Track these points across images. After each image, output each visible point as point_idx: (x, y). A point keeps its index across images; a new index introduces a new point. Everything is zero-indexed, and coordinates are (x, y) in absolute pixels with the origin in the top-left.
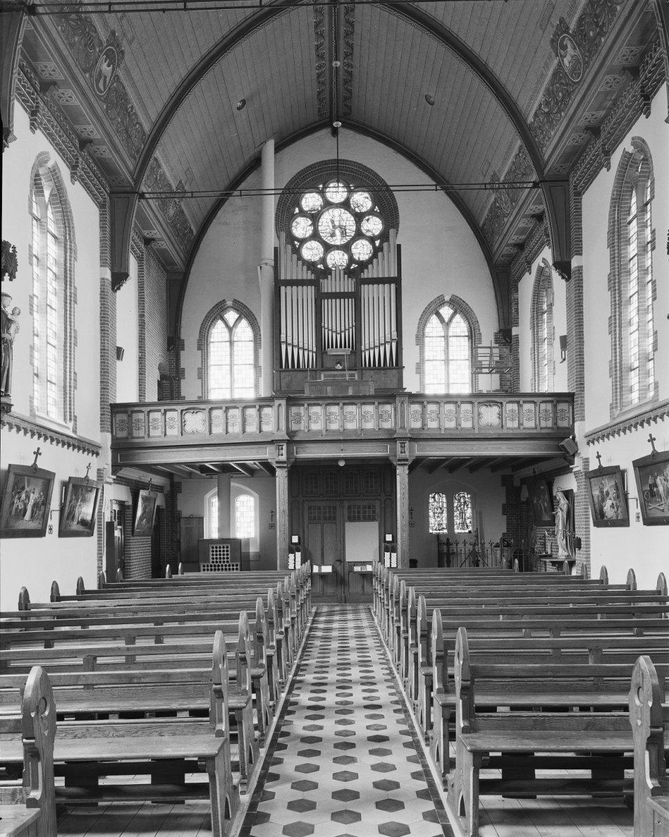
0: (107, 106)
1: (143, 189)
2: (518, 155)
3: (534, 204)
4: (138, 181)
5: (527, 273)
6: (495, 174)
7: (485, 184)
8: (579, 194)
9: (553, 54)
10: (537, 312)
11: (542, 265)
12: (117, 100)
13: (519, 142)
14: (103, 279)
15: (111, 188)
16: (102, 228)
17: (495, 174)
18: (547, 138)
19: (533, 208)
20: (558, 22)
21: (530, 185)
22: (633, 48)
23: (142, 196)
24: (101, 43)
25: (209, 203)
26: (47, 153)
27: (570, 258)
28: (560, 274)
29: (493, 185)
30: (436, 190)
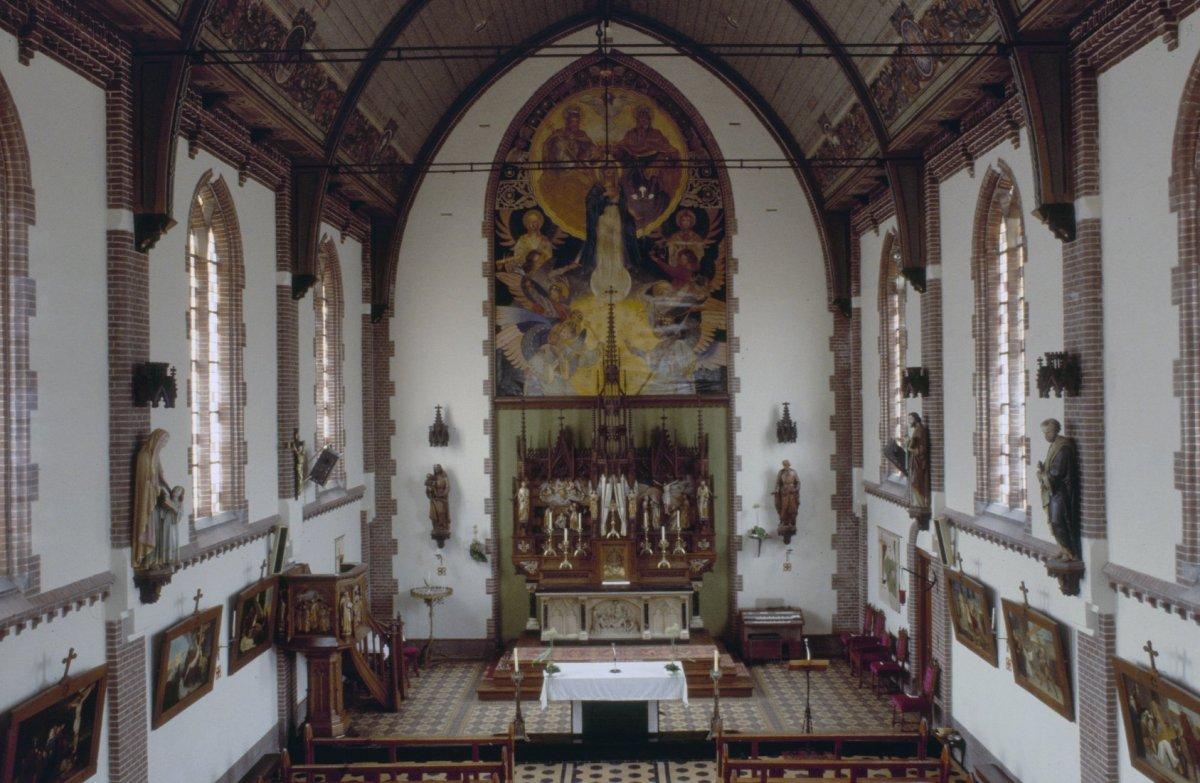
6: (824, 115)
9: (895, 32)
13: (854, 99)
14: (280, 288)
16: (364, 258)
17: (824, 115)
27: (1073, 197)
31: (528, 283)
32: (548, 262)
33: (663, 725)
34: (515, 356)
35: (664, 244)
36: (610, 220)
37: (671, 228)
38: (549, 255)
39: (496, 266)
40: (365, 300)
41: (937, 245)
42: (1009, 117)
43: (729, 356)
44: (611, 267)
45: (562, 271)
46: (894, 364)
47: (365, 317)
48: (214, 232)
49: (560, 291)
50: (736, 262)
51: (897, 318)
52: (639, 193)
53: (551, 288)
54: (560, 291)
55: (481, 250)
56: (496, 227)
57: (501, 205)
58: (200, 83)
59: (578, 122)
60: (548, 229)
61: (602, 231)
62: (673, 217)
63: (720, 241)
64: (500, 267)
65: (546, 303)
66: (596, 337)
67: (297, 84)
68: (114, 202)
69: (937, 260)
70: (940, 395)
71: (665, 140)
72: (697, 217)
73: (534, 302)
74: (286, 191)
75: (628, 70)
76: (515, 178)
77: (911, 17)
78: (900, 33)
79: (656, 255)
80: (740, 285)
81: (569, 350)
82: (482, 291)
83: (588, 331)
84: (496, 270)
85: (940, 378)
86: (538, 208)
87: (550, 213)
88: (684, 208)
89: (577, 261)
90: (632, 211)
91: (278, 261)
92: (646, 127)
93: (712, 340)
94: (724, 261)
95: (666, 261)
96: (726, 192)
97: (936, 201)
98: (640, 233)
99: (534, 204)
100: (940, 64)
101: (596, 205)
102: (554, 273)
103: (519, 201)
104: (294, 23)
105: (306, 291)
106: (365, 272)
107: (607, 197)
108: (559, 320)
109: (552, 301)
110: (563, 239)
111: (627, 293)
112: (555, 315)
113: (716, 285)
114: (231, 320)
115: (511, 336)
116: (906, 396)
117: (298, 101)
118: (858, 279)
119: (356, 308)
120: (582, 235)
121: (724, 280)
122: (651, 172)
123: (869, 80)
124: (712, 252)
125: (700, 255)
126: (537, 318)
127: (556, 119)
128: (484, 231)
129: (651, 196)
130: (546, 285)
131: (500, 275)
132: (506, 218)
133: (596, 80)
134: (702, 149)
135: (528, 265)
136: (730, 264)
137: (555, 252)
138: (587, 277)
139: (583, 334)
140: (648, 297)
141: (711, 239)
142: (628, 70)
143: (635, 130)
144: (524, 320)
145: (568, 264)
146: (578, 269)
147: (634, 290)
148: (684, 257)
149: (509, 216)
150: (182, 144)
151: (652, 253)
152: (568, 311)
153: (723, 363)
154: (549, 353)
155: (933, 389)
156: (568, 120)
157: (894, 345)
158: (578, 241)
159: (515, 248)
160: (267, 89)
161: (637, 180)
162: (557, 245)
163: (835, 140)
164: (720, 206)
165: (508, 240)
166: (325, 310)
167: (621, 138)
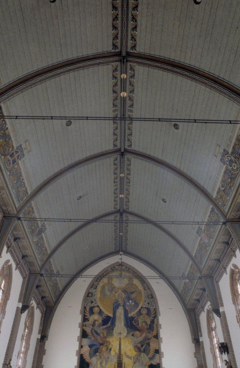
0: (10, 174)
1: (21, 216)
2: (210, 216)
3: (215, 254)
4: (18, 212)
5: (234, 258)
7: (180, 277)
8: (217, 282)
9: (198, 236)
10: (210, 330)
11: (233, 268)
12: (40, 245)
13: (191, 262)
14: (18, 308)
15: (30, 271)
16: (41, 319)
17: (183, 273)
18: (225, 202)
19: (200, 287)
20: (223, 151)
21: (198, 278)
22: (236, 213)
23: (19, 219)
24: (13, 148)
25: (68, 279)
26: (10, 260)
28: (216, 314)
29: (183, 277)
30: (160, 279)
31: (93, 331)
32: (100, 324)
33: (150, 52)
34: (87, 357)
35: (137, 319)
36: (120, 311)
37: (139, 313)
38: (101, 321)
39: (83, 324)
40: (39, 333)
41: (221, 300)
42: (232, 250)
43: (160, 359)
44: (120, 326)
45: (105, 327)
46: (217, 357)
47: (38, 339)
48: (5, 281)
49: (103, 334)
50: (160, 325)
51: (214, 332)
52: (129, 303)
53: (100, 333)
54: (103, 334)
55: (79, 319)
56: (85, 312)
57: (87, 305)
58: (15, 233)
59: (112, 281)
60: (100, 313)
61: (118, 314)
62: (140, 310)
63: (155, 318)
64: (84, 325)
65: (98, 338)
66: (115, 351)
67: (38, 244)
68: (19, 301)
69: (222, 305)
70: (233, 351)
71: (137, 287)
72: (148, 310)
73: (95, 337)
74: (26, 279)
75: (126, 267)
76: (92, 297)
77: (202, 230)
78: (200, 236)
79: (135, 323)
80: (163, 334)
81: (105, 355)
82: (77, 332)
83: (112, 348)
84: (83, 326)
85: (231, 345)
86: (98, 306)
87: (101, 308)
88: (143, 308)
89: (109, 323)
90: (127, 308)
91: (19, 299)
92: (132, 283)
93: (154, 353)
94: (157, 325)
95: (138, 325)
96: (156, 303)
97: (219, 288)
98: (129, 315)
99: (97, 305)
100: (211, 239)
101: (116, 306)
102: (102, 327)
103: (92, 304)
104: (42, 226)
105: (25, 311)
106: (41, 324)
107: (119, 304)
108: (102, 344)
109: (101, 337)
110: (105, 316)
111: (125, 334)
112: (101, 342)
113: (154, 333)
114: (2, 309)
115: (86, 350)
116: (221, 353)
117: (37, 250)
118: (201, 331)
119: (36, 335)
120: (111, 315)
121: (157, 332)
122: (133, 296)
123: (194, 255)
124: (153, 322)
125: (149, 323)
126: (95, 343)
127: (105, 280)
128: (81, 313)
129: (133, 304)
130: (99, 332)
131: (84, 328)
132: (88, 309)
133: (117, 270)
134: (148, 290)
135: (93, 325)
136: (158, 326)
137: (103, 321)
138: (113, 330)
139: (110, 349)
140: (132, 337)
141: (153, 315)
142: (126, 267)
143: (128, 284)
144: (91, 344)
145: (107, 325)
146: (109, 327)
147: (128, 333)
148: (144, 323)
149: (89, 308)
150: (5, 248)
151: (133, 322)
152: (106, 341)
153: (158, 362)
154: (98, 357)
155: (229, 349)
156: (109, 280)
157: (216, 349)
158: (110, 317)
159: (90, 319)
160: (30, 240)
161: (129, 299)
162: (103, 318)
163: (187, 281)
164: (154, 307)
165: (87, 316)
166: (26, 330)
167: (124, 286)
